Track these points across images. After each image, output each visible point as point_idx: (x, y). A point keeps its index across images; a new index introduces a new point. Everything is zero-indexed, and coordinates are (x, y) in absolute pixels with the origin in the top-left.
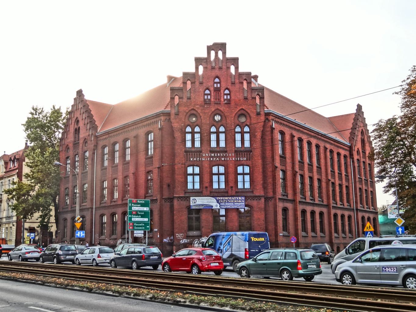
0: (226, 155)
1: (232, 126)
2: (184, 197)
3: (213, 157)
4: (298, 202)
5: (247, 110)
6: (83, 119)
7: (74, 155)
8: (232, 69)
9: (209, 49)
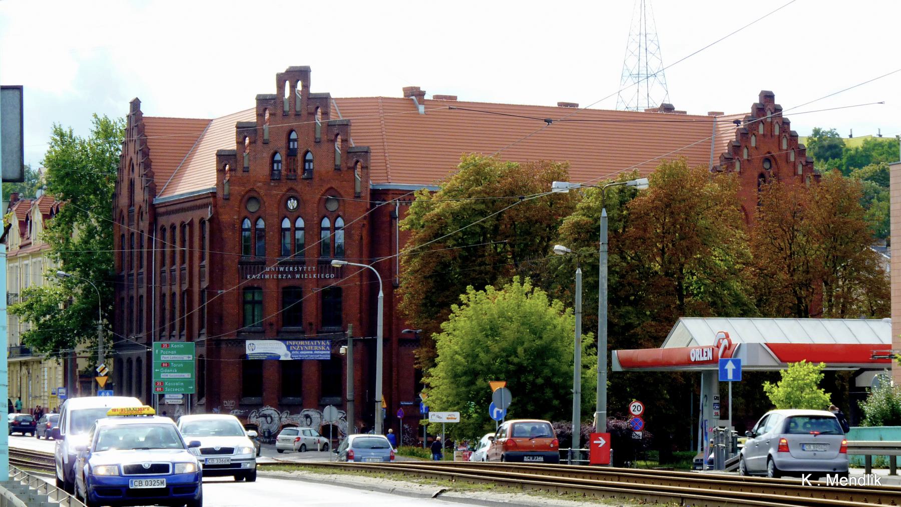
0: (303, 269)
3: (282, 273)
9: (281, 80)
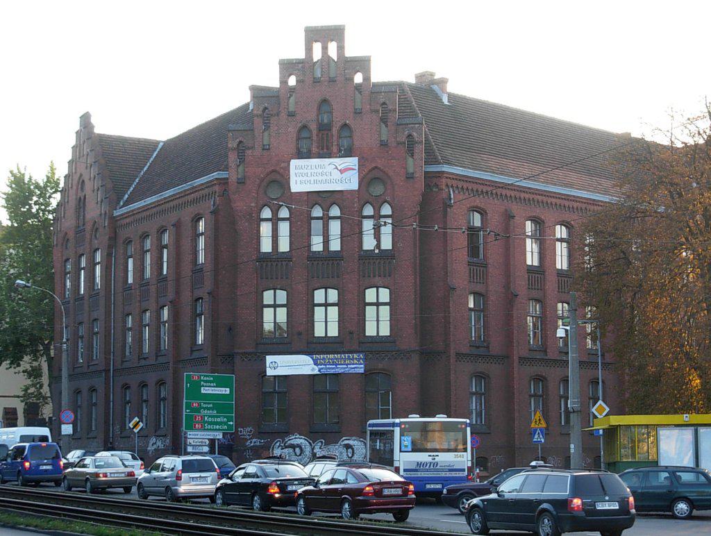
1: (354, 204)
2: (255, 354)
4: (516, 358)
5: (386, 170)
6: (90, 179)
7: (92, 250)
8: (358, 78)
